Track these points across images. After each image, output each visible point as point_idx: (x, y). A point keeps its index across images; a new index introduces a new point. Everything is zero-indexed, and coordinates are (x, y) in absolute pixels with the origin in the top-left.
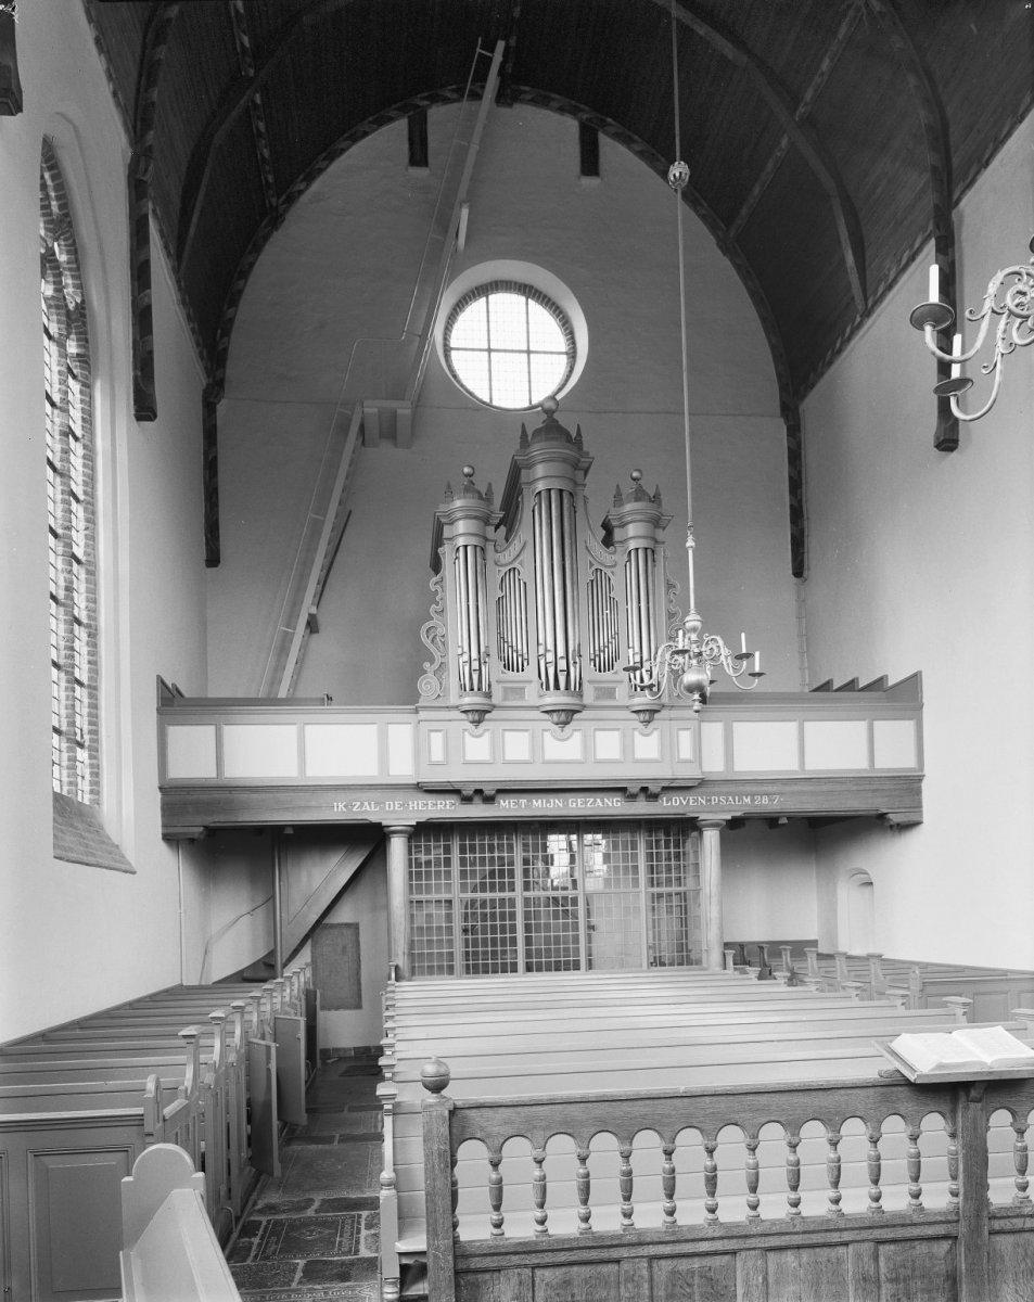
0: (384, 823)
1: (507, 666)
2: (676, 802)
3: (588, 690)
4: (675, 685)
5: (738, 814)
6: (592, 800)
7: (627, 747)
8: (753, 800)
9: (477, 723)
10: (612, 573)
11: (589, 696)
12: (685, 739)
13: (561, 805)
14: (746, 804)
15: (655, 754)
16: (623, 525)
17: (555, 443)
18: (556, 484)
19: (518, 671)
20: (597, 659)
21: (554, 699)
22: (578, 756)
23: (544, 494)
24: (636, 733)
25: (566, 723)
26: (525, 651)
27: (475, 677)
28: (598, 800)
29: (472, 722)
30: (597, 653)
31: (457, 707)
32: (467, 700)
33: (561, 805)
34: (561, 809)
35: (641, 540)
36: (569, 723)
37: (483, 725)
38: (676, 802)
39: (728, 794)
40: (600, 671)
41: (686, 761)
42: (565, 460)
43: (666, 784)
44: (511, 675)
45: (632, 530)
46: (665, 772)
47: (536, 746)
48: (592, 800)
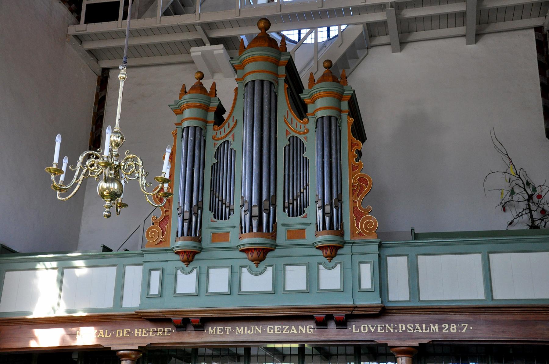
0: (114, 348)
1: (216, 216)
2: (364, 330)
3: (281, 233)
4: (357, 225)
5: (425, 341)
6: (287, 327)
7: (313, 279)
8: (440, 329)
9: (331, 257)
10: (305, 138)
11: (281, 238)
12: (366, 271)
13: (260, 332)
14: (434, 332)
15: (337, 285)
16: (313, 101)
17: (259, 48)
18: (259, 77)
19: (225, 219)
20: (295, 203)
21: (325, 238)
22: (269, 287)
23: (250, 85)
24: (244, 270)
25: (263, 259)
26: (228, 201)
27: (327, 219)
28: (293, 327)
29: (184, 261)
30: (291, 201)
31: (313, 244)
32: (321, 238)
33: (260, 332)
34: (260, 335)
35: (325, 111)
36: (192, 261)
37: (335, 260)
38: (364, 330)
39: (414, 322)
40: (289, 215)
41: (367, 291)
42: (265, 59)
43: (349, 312)
44: (220, 223)
45: (320, 103)
46: (346, 301)
47: (234, 280)
48: (287, 327)
